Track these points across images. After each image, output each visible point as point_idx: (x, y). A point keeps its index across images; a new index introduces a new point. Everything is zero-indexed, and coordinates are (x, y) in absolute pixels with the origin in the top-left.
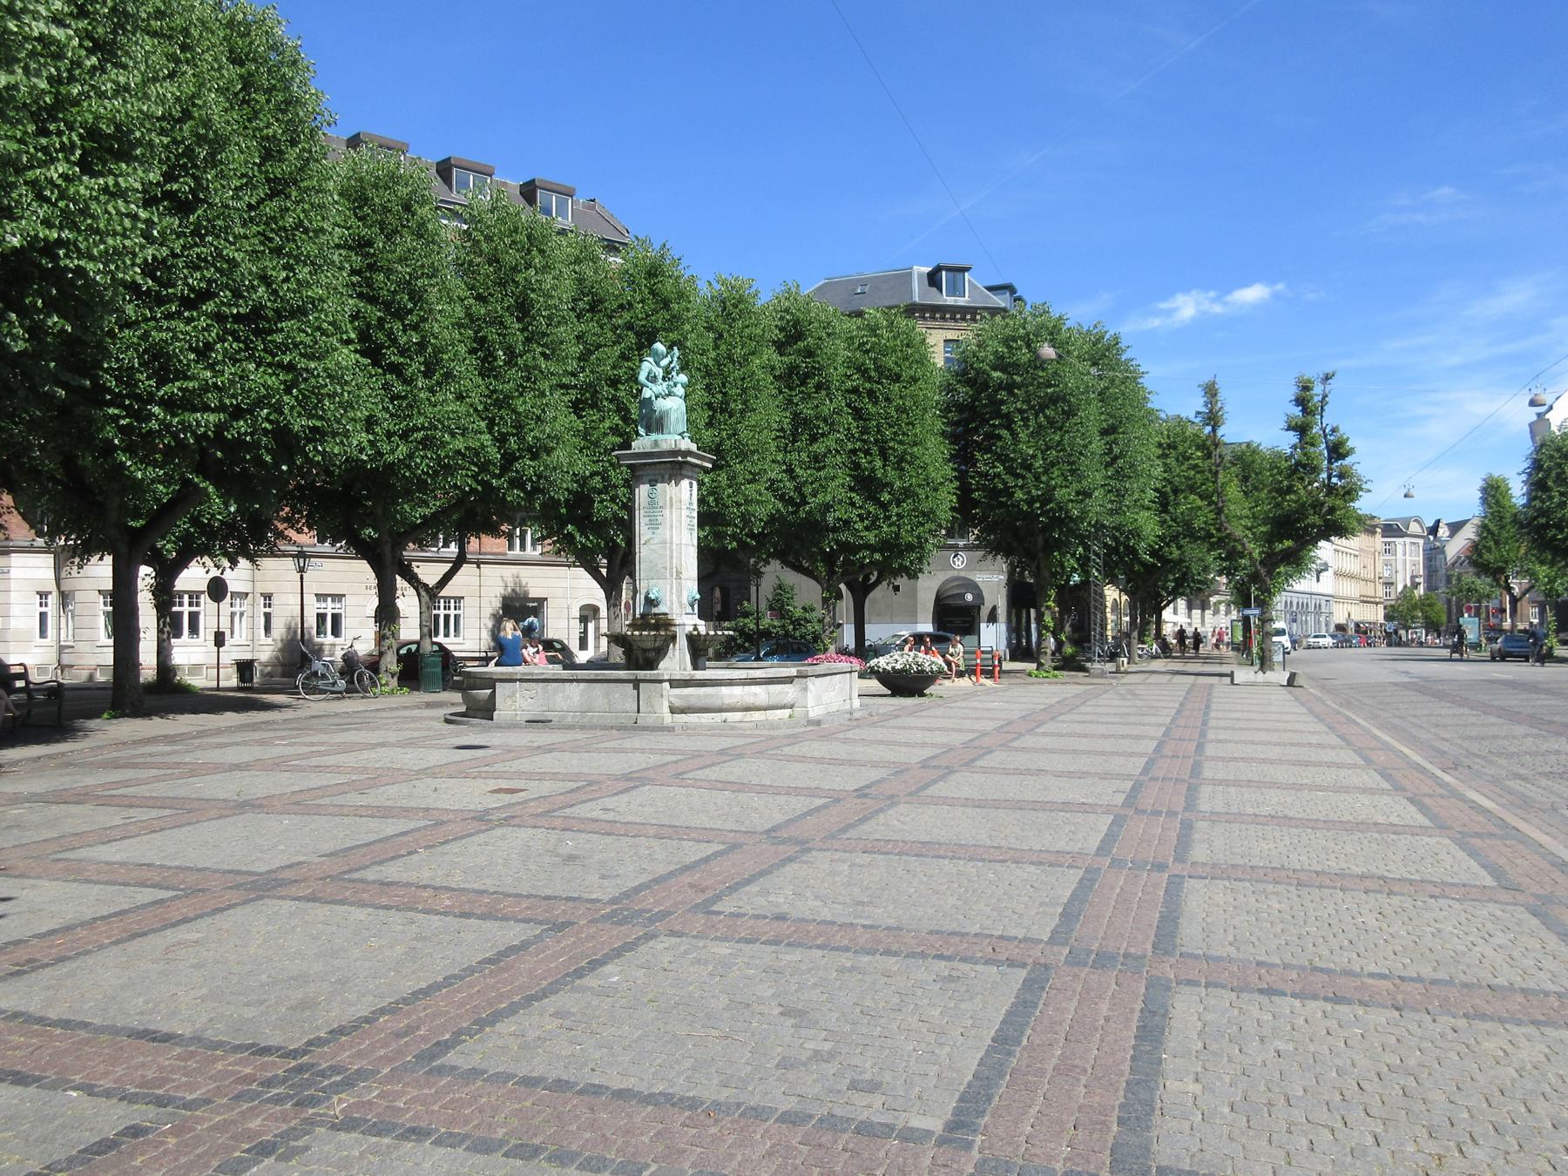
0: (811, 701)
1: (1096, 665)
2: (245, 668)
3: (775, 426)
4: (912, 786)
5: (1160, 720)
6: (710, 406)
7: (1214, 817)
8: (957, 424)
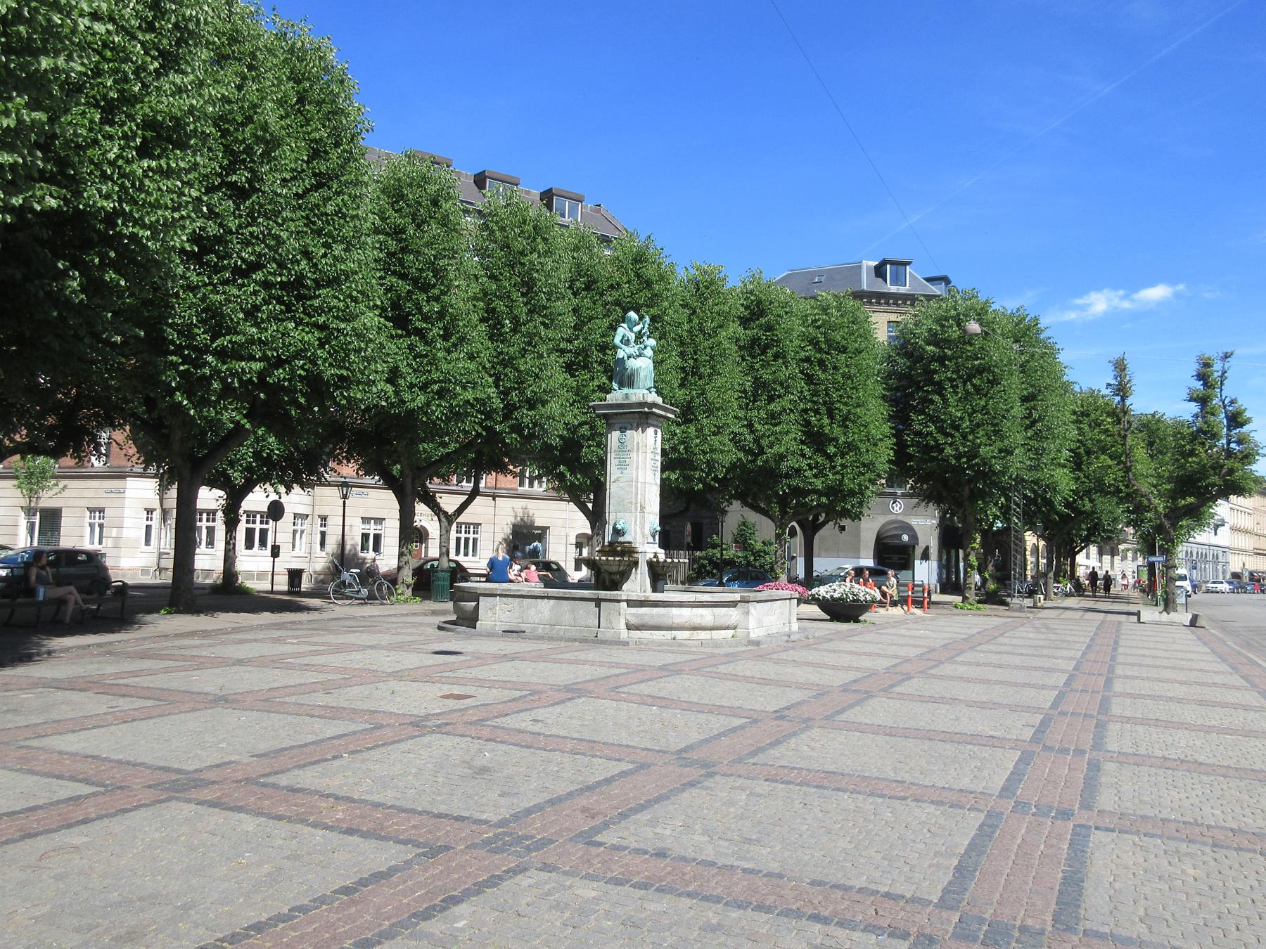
0: (752, 623)
1: (1015, 601)
2: (295, 575)
3: (737, 387)
4: (857, 695)
5: (1071, 654)
6: (683, 369)
7: (1122, 758)
8: (897, 389)
